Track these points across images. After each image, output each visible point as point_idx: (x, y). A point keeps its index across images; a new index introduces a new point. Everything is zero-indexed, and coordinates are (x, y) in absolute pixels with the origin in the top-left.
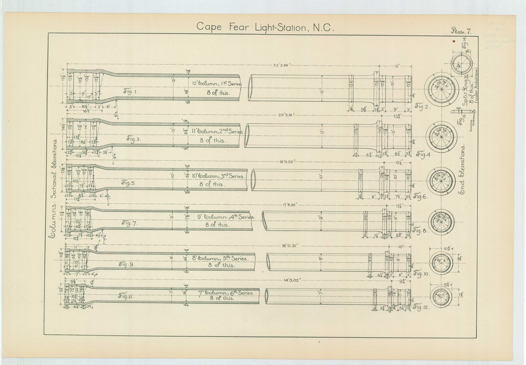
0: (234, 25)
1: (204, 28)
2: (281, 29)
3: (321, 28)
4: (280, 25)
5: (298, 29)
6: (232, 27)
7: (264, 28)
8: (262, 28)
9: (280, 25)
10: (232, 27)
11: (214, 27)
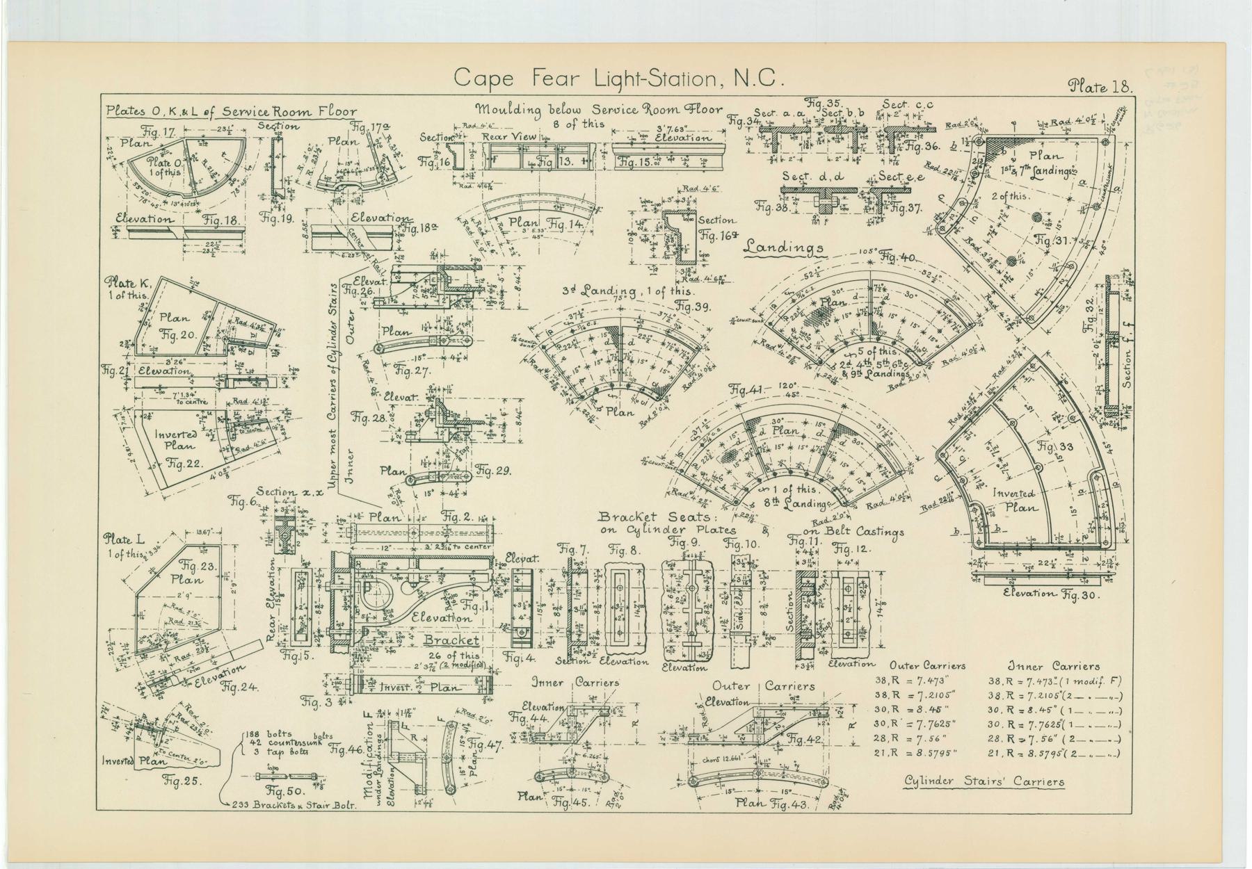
0: (542, 73)
1: (472, 82)
2: (656, 81)
3: (753, 79)
4: (654, 72)
5: (698, 80)
6: (539, 80)
7: (617, 81)
8: (610, 81)
9: (654, 72)
10: (539, 80)
11: (495, 80)
